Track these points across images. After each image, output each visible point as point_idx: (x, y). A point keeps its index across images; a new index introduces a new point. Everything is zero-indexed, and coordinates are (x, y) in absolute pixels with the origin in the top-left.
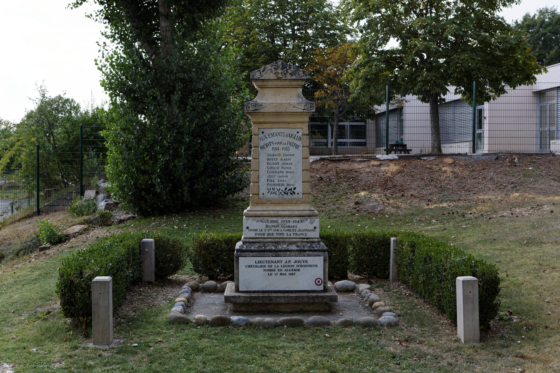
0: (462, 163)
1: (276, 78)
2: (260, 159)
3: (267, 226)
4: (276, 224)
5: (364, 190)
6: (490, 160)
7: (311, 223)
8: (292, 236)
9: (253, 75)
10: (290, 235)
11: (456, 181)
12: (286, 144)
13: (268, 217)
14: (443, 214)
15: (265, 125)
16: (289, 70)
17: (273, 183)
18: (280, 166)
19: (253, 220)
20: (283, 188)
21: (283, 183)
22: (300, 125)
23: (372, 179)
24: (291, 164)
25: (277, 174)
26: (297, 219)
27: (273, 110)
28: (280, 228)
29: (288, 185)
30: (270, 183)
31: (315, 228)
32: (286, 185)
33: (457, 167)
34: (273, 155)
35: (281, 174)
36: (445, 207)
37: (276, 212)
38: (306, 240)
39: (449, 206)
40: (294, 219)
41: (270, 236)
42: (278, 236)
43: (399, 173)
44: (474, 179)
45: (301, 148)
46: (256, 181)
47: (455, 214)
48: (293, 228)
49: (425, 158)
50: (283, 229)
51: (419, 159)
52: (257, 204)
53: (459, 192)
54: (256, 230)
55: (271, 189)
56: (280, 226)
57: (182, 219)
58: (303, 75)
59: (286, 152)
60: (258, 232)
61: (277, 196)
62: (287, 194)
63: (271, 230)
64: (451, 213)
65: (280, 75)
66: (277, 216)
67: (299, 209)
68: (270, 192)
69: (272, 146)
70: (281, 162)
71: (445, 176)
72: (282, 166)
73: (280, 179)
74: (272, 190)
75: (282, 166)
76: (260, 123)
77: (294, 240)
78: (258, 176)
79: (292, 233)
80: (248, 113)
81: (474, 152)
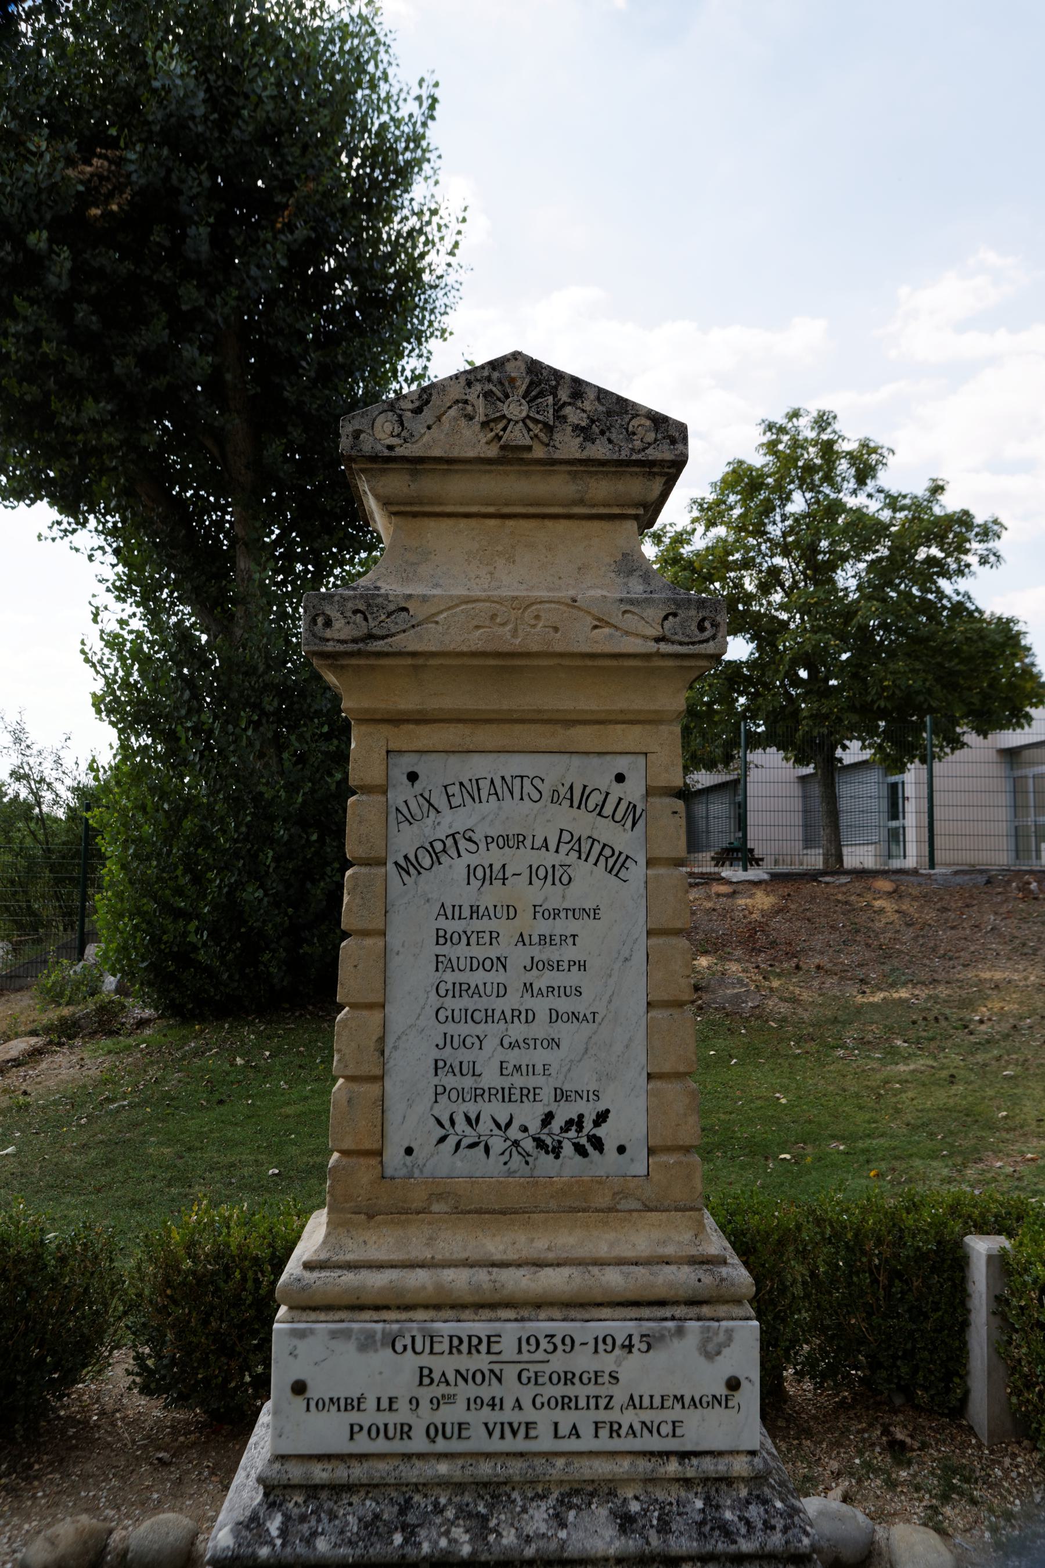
0: (915, 892)
1: (493, 452)
2: (395, 938)
3: (425, 1376)
4: (481, 1362)
5: (705, 953)
6: (975, 886)
7: (710, 1352)
8: (587, 1442)
9: (357, 434)
10: (575, 1432)
11: (910, 933)
12: (552, 845)
13: (437, 1307)
14: (914, 1022)
15: (424, 730)
16: (568, 410)
17: (468, 1082)
18: (514, 978)
19: (334, 1335)
20: (529, 1115)
21: (531, 1082)
22: (632, 737)
23: (721, 928)
24: (582, 966)
25: (493, 1030)
26: (620, 1327)
27: (475, 640)
28: (510, 1390)
29: (561, 1095)
30: (450, 1081)
31: (733, 1384)
32: (546, 1094)
33: (907, 901)
34: (474, 910)
35: (517, 1031)
36: (907, 1000)
37: (482, 1276)
38: (673, 1467)
39: (917, 997)
40: (600, 1328)
41: (441, 1445)
42: (496, 1445)
43: (778, 912)
44: (953, 928)
45: (637, 872)
46: (365, 1070)
47: (944, 1023)
48: (592, 1390)
49: (827, 879)
50: (526, 1394)
51: (816, 880)
52: (370, 1217)
53: (927, 962)
54: (354, 1404)
55: (460, 1119)
56: (510, 1373)
57: (268, 1032)
58: (651, 437)
59: (553, 896)
60: (368, 1417)
61: (493, 1166)
62: (557, 1151)
63: (450, 1399)
64: (931, 1018)
65: (517, 435)
66: (493, 1306)
67: (629, 1253)
68: (451, 1141)
69: (467, 859)
70: (519, 957)
71: (884, 921)
72: (529, 977)
73: (514, 1057)
74: (461, 1124)
75: (529, 977)
76: (397, 720)
77: (602, 1468)
78: (382, 1039)
79: (585, 1420)
80: (323, 655)
81: (932, 865)
